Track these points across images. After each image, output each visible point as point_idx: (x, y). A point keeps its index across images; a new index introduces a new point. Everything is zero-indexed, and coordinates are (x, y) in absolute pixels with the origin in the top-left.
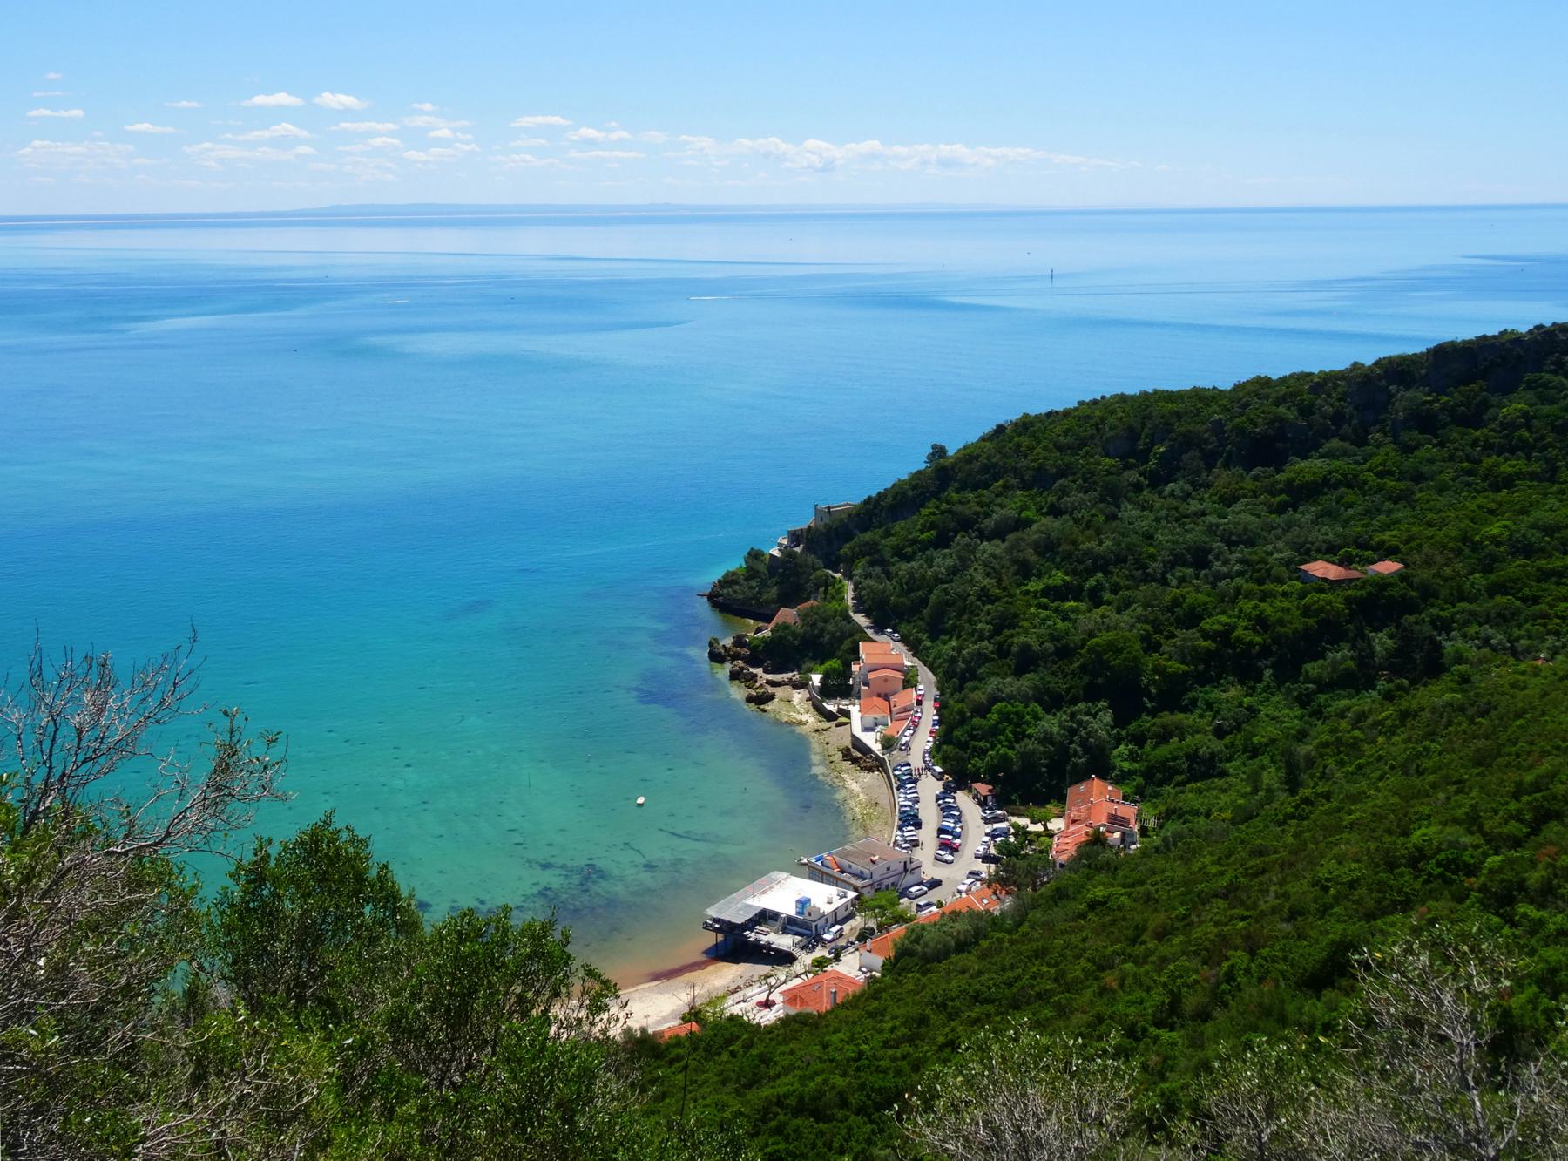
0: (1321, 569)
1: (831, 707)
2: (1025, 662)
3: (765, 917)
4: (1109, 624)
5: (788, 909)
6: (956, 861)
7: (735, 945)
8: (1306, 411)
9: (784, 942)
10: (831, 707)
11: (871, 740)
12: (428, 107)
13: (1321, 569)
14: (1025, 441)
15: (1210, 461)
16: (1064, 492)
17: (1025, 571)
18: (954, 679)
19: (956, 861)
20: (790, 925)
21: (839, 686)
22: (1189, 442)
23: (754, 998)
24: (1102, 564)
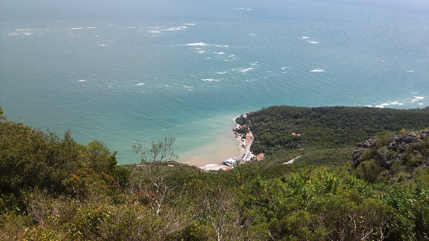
0: (294, 134)
1: (243, 140)
2: (261, 140)
3: (228, 162)
4: (269, 136)
5: (230, 162)
6: (249, 156)
7: (225, 164)
8: (302, 113)
9: (229, 164)
10: (243, 140)
11: (245, 145)
12: (201, 52)
13: (294, 134)
14: (272, 110)
15: (290, 117)
16: (274, 118)
17: (266, 128)
18: (255, 139)
19: (249, 156)
20: (230, 163)
21: (244, 137)
22: (289, 114)
23: (224, 168)
24: (273, 129)
